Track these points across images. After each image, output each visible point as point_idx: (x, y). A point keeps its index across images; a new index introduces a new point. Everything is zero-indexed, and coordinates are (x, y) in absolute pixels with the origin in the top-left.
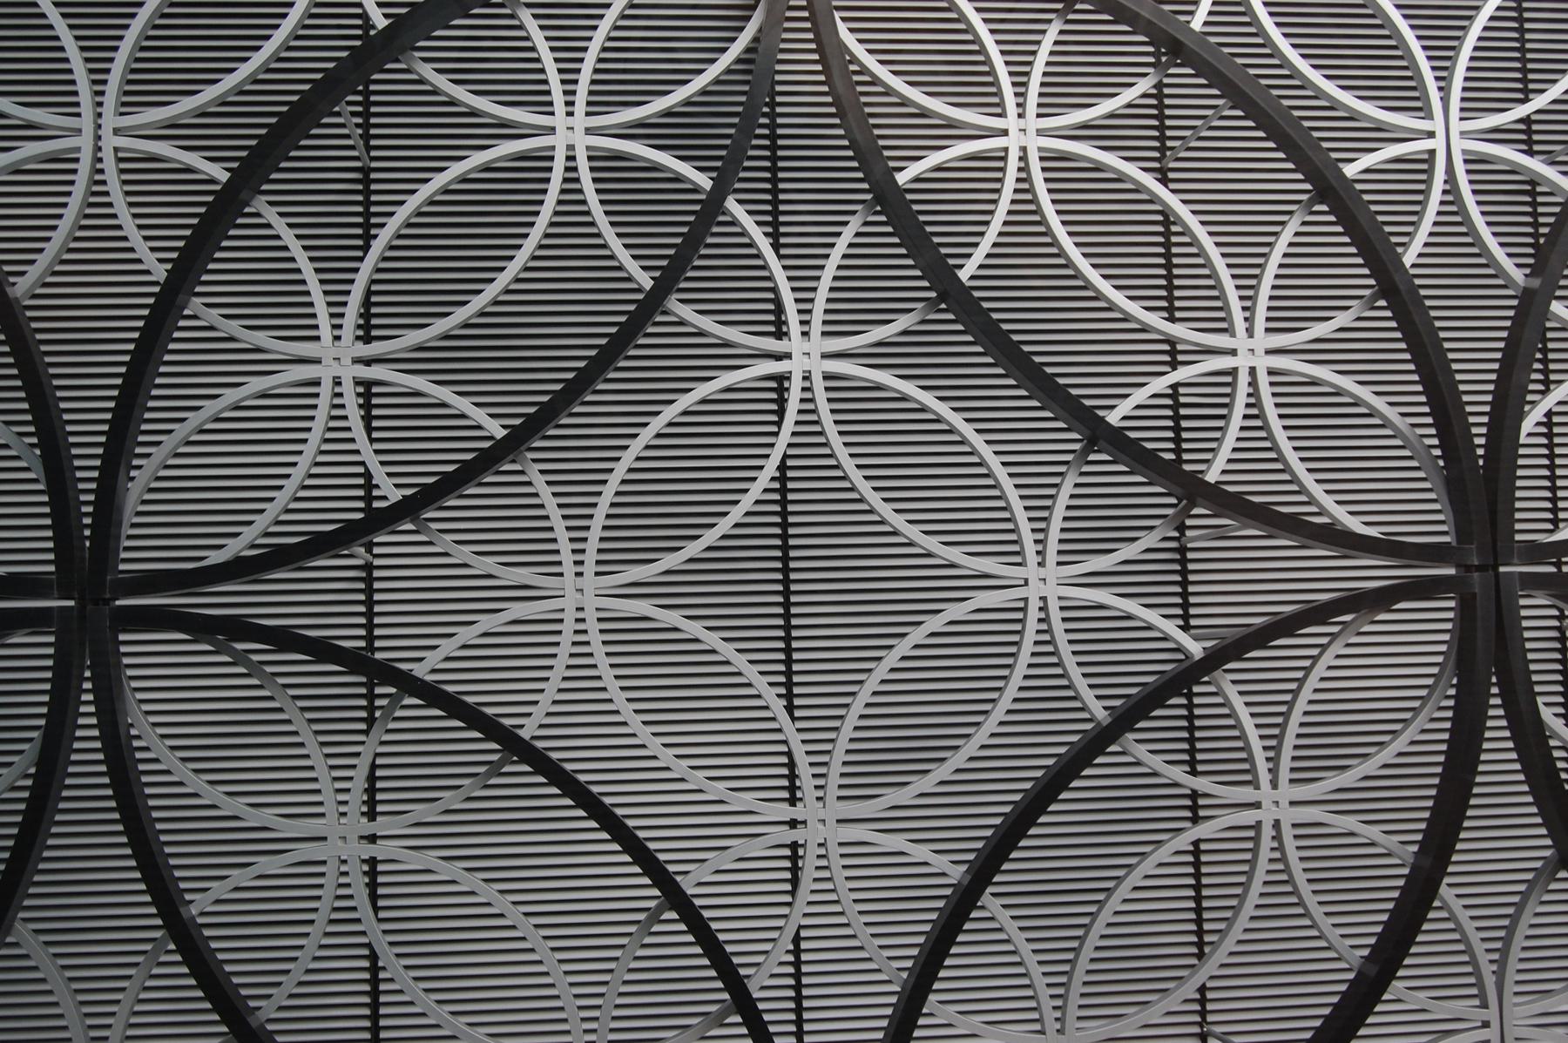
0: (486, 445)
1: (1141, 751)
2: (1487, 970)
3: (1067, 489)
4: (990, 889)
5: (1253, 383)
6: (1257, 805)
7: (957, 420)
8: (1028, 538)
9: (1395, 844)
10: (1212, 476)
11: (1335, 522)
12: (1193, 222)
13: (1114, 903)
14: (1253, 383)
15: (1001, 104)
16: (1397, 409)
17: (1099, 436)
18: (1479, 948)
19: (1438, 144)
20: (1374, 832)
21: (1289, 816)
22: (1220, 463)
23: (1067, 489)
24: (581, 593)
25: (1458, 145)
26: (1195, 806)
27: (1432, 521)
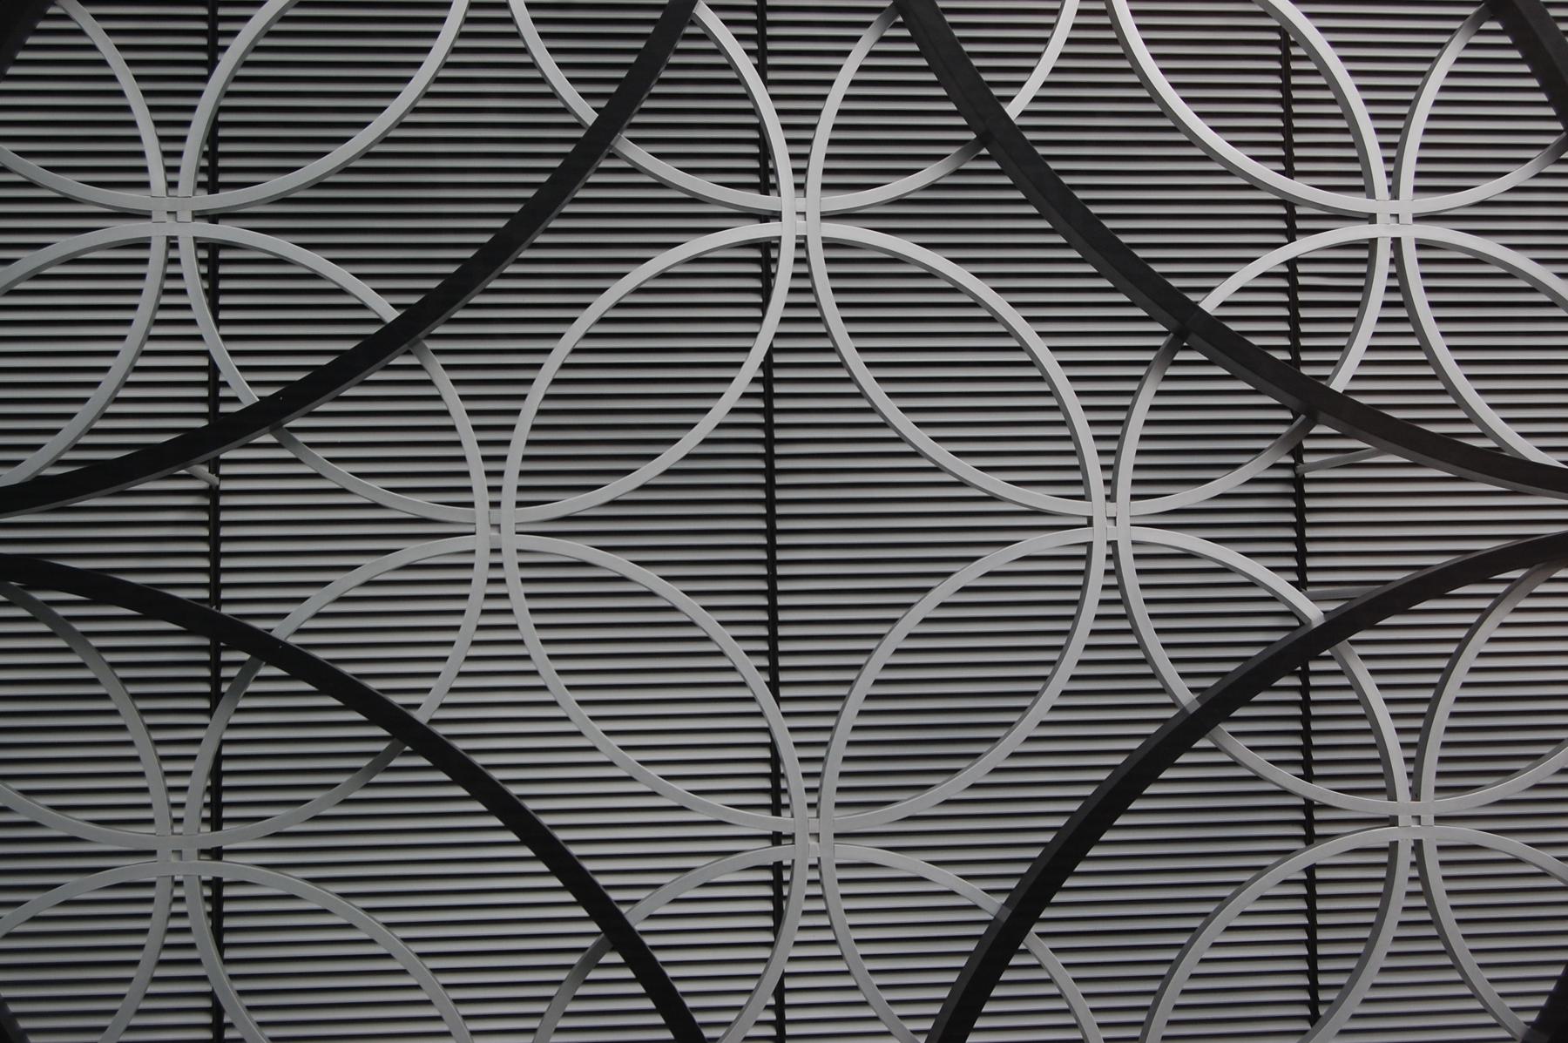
0: (372, 330)
1: (1240, 747)
3: (1146, 398)
4: (1037, 928)
5: (1397, 260)
6: (1392, 821)
7: (1000, 304)
11: (1503, 446)
13: (1201, 949)
14: (1397, 260)
21: (1434, 835)
22: (1350, 366)
23: (1146, 398)
24: (497, 529)
26: (1310, 823)
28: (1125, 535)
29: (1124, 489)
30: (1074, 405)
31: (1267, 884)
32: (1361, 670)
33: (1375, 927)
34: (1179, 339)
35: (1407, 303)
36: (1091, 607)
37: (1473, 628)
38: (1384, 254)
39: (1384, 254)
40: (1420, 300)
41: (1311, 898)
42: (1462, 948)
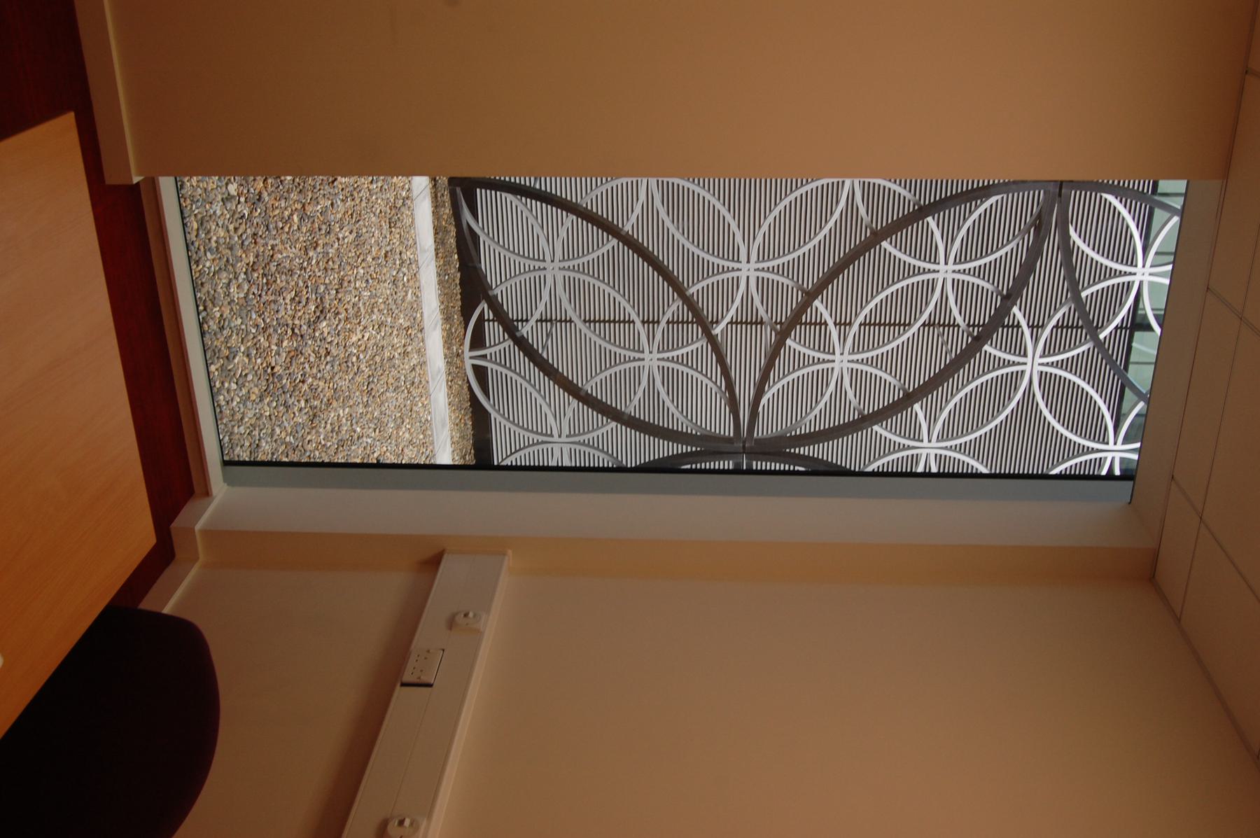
1: (674, 307)
2: (581, 439)
5: (829, 361)
7: (1002, 417)
8: (860, 357)
9: (632, 407)
10: (789, 342)
12: (909, 334)
13: (608, 290)
14: (829, 361)
15: (960, 262)
16: (812, 420)
17: (810, 296)
18: (590, 436)
19: (1111, 446)
25: (924, 452)
26: (650, 322)
27: (763, 430)
28: (646, 363)
29: (662, 364)
30: (879, 351)
31: (629, 309)
32: (698, 345)
34: (874, 233)
36: (722, 262)
38: (830, 357)
39: (830, 357)
41: (624, 322)
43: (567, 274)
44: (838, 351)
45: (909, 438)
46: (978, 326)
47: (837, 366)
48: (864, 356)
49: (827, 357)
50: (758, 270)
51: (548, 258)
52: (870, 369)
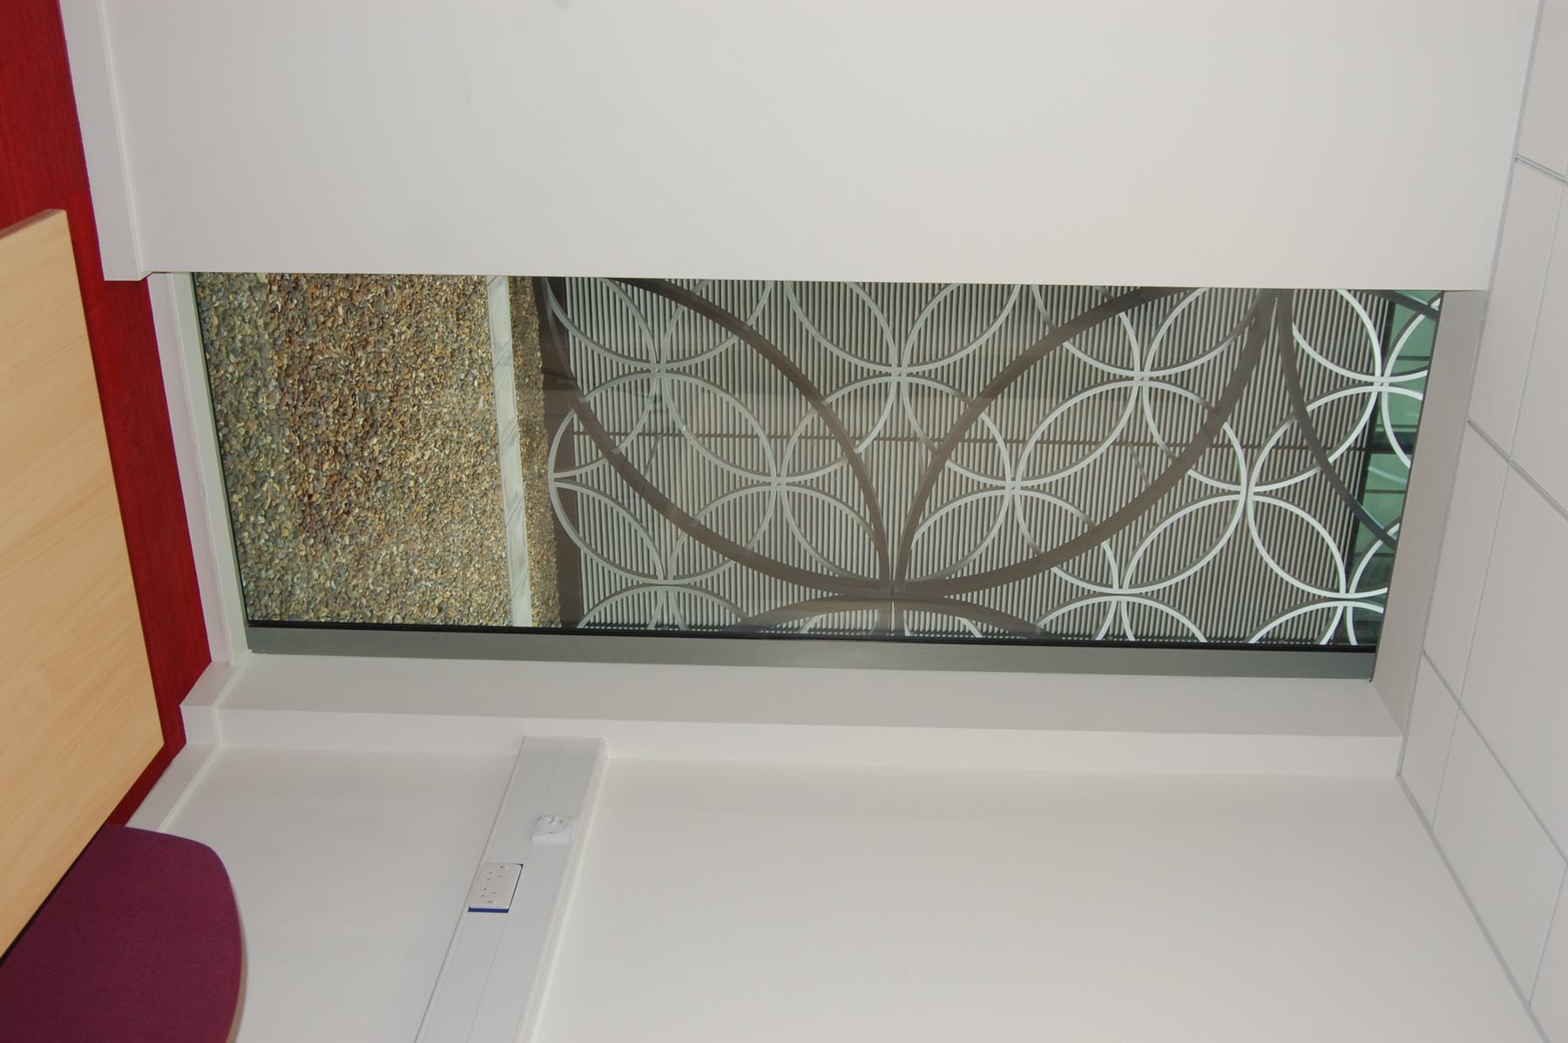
2: (691, 581)
5: (997, 488)
6: (899, 365)
8: (1035, 483)
9: (757, 540)
12: (1097, 455)
14: (997, 488)
16: (982, 554)
19: (1115, 589)
20: (765, 526)
21: (893, 381)
22: (954, 468)
25: (1114, 599)
32: (837, 466)
33: (734, 465)
34: (1054, 331)
35: (979, 491)
36: (867, 365)
37: (852, 508)
40: (980, 496)
42: (725, 500)
43: (676, 377)
44: (1008, 476)
45: (874, 362)
46: (1181, 445)
47: (1007, 493)
48: (1041, 482)
49: (996, 483)
50: (910, 375)
51: (653, 358)
52: (1048, 498)
